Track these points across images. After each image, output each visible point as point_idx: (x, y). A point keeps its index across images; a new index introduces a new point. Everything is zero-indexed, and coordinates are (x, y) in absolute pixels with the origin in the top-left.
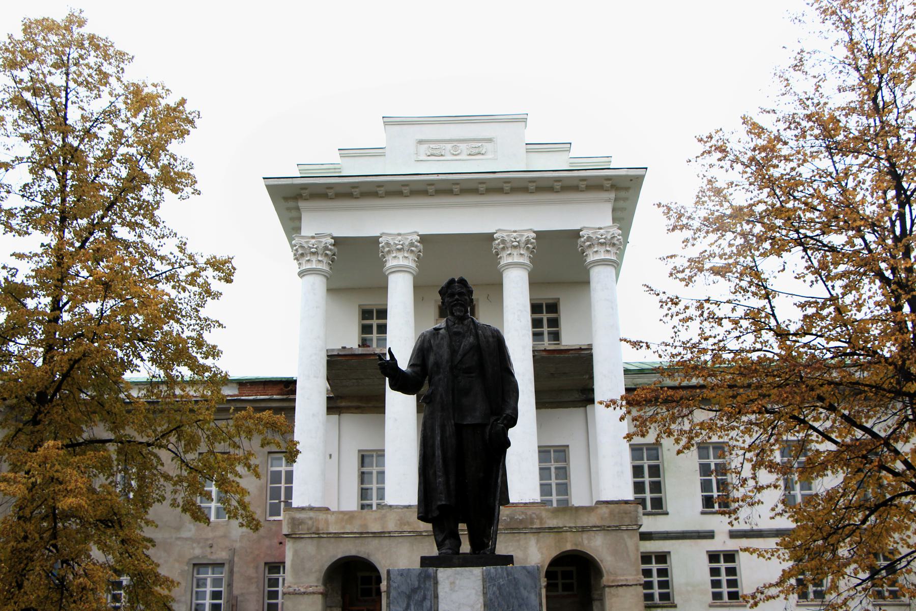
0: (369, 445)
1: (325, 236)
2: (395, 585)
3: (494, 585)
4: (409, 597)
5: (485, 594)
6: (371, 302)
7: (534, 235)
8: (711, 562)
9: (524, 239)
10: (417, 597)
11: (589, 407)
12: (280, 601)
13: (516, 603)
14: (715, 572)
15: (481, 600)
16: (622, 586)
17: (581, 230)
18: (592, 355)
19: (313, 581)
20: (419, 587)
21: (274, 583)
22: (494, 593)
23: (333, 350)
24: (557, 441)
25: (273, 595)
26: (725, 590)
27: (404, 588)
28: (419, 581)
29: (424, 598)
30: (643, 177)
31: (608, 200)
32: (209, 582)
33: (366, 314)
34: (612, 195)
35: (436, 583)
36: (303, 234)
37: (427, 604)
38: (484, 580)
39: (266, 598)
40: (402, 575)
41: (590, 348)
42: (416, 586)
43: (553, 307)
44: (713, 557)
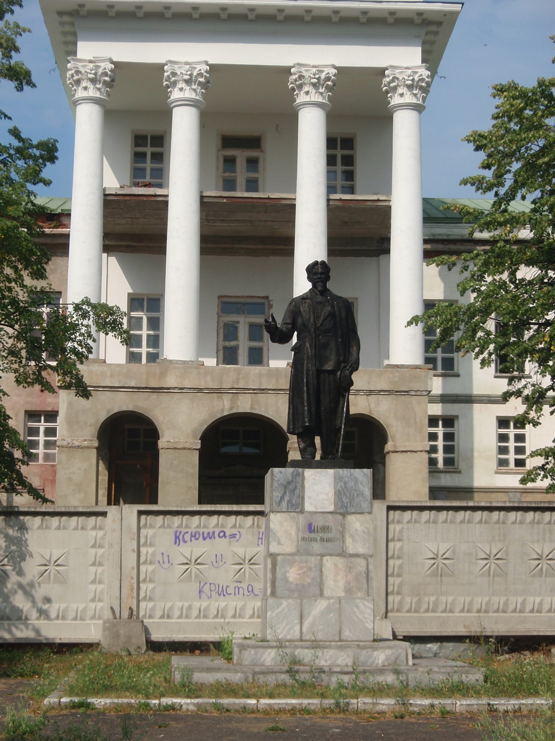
1: (104, 61)
2: (276, 479)
3: (342, 481)
4: (285, 487)
5: (335, 487)
6: (149, 128)
7: (334, 71)
8: (500, 427)
9: (323, 76)
10: (291, 487)
11: (382, 257)
13: (356, 494)
14: (503, 438)
15: (333, 491)
16: (406, 452)
17: (386, 69)
18: (390, 207)
19: (88, 436)
20: (292, 481)
22: (341, 486)
26: (512, 457)
27: (282, 481)
28: (292, 477)
29: (296, 488)
31: (418, 37)
33: (139, 140)
34: (423, 31)
36: (80, 56)
37: (297, 492)
38: (335, 477)
42: (290, 480)
43: (348, 143)
44: (503, 422)
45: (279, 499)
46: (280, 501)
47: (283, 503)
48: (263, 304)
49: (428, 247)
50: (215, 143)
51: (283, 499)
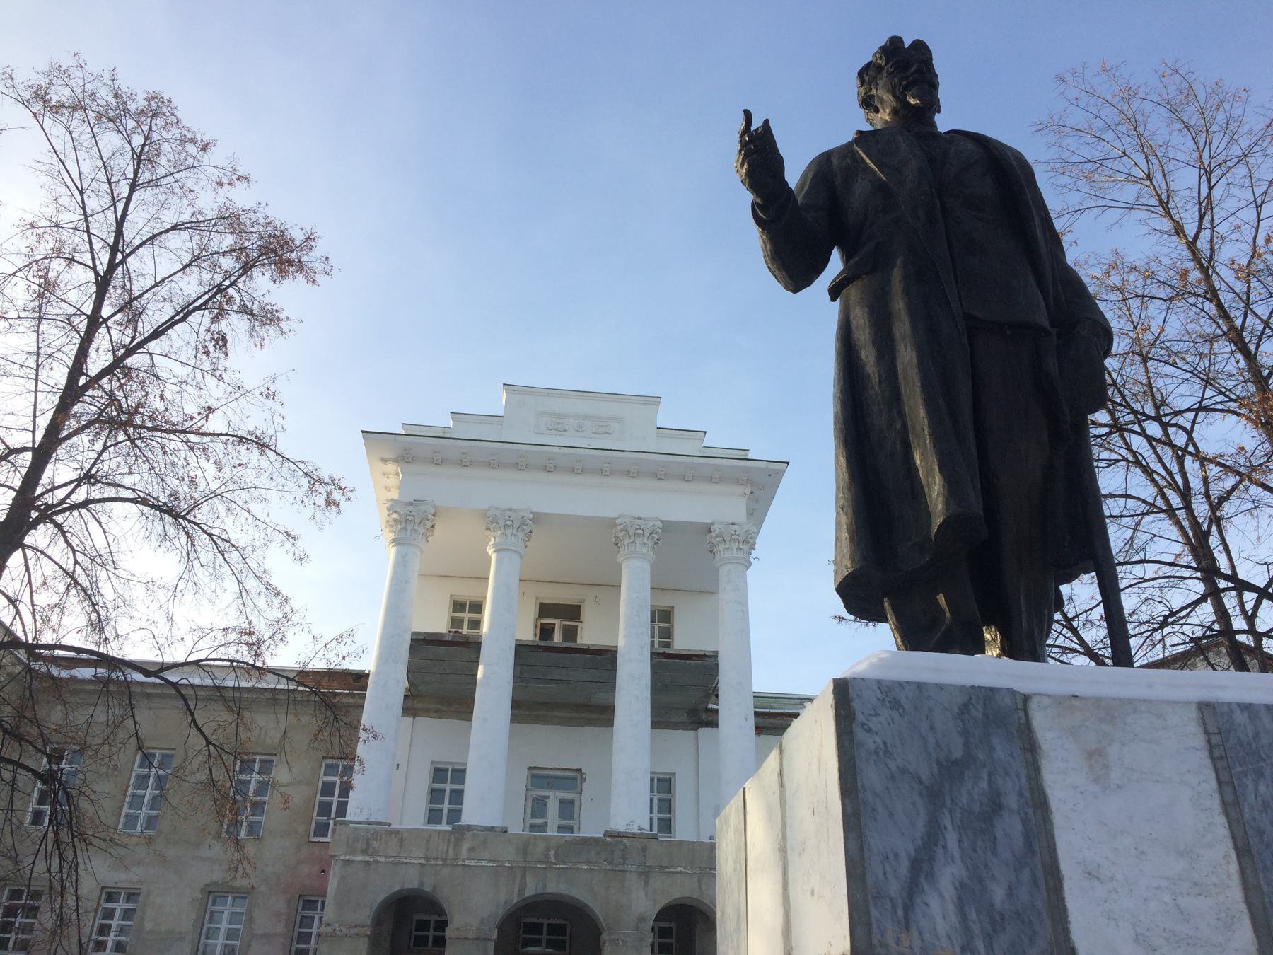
0: (446, 757)
2: (870, 742)
4: (934, 795)
7: (660, 525)
10: (971, 792)
11: (704, 732)
12: (312, 946)
21: (306, 922)
23: (419, 633)
24: (665, 768)
25: (305, 938)
28: (965, 734)
29: (995, 805)
30: (780, 474)
32: (225, 917)
35: (1030, 748)
37: (1010, 827)
39: (295, 942)
40: (896, 705)
41: (715, 656)
45: (904, 867)
46: (913, 889)
47: (935, 906)
48: (575, 779)
49: (761, 720)
50: (522, 779)
51: (931, 876)
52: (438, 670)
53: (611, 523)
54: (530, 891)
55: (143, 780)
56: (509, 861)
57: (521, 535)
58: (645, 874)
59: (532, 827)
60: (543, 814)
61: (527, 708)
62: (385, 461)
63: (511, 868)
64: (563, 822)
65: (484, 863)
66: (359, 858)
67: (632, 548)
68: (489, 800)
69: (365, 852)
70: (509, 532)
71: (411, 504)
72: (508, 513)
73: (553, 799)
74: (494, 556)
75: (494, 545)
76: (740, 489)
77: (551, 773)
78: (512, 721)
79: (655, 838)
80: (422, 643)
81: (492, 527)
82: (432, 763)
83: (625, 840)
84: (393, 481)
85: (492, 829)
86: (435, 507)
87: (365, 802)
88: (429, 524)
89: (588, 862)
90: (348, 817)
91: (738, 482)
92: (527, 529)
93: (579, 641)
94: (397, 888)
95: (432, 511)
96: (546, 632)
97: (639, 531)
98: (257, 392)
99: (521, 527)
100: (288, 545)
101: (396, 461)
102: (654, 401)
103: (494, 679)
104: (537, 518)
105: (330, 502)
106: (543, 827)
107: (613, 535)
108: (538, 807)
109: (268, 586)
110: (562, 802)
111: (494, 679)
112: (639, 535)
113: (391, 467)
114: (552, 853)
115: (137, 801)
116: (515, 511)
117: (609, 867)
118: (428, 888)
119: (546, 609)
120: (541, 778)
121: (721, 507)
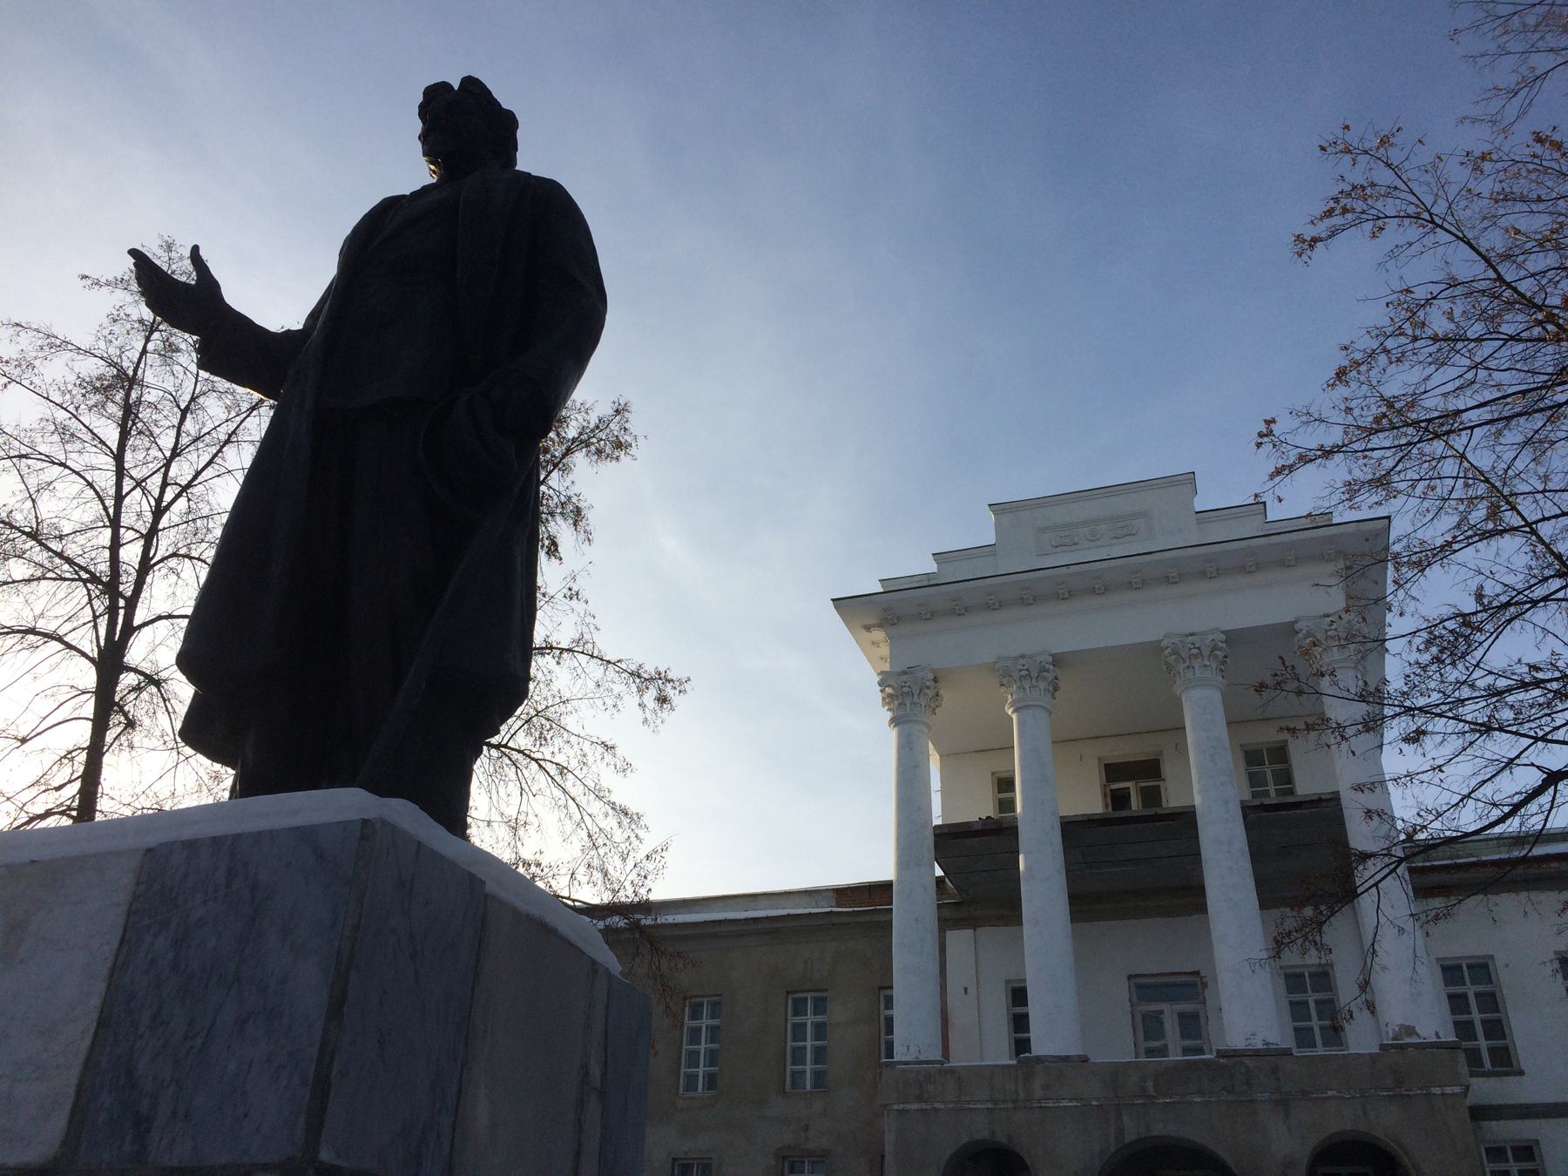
7: (1223, 637)
48: (1195, 985)
52: (970, 866)
53: (1155, 648)
54: (1130, 1136)
55: (695, 1034)
56: (1097, 1099)
57: (1042, 685)
58: (1283, 1103)
59: (1150, 1052)
60: (1160, 1035)
61: (1086, 904)
62: (868, 628)
63: (1100, 1107)
64: (1188, 1043)
65: (1065, 1103)
66: (915, 1106)
67: (1189, 675)
68: (1248, 1013)
69: (919, 1099)
70: (1027, 685)
71: (905, 673)
72: (1022, 661)
73: (1170, 1013)
74: (1014, 717)
75: (1012, 705)
76: (1330, 568)
77: (1171, 980)
78: (1073, 920)
79: (1287, 1053)
80: (950, 840)
81: (1005, 681)
82: (1007, 982)
83: (1247, 1061)
84: (885, 650)
85: (1067, 1059)
86: (933, 671)
87: (912, 1037)
88: (931, 693)
89: (1201, 1093)
90: (896, 1059)
91: (1322, 558)
92: (1050, 676)
93: (1164, 804)
94: (965, 1140)
95: (931, 676)
96: (1119, 800)
97: (1194, 651)
98: (560, 596)
99: (1044, 675)
100: (608, 757)
101: (880, 626)
102: (1188, 480)
103: (1040, 870)
104: (1058, 660)
105: (662, 700)
106: (1163, 1051)
107: (1161, 662)
108: (1151, 1026)
109: (613, 806)
110: (1181, 1016)
111: (1040, 870)
112: (1196, 656)
113: (878, 635)
114: (1150, 1084)
115: (693, 1059)
116: (1030, 657)
117: (1230, 1098)
118: (1001, 1138)
119: (1113, 771)
120: (1146, 988)
121: (1306, 599)
